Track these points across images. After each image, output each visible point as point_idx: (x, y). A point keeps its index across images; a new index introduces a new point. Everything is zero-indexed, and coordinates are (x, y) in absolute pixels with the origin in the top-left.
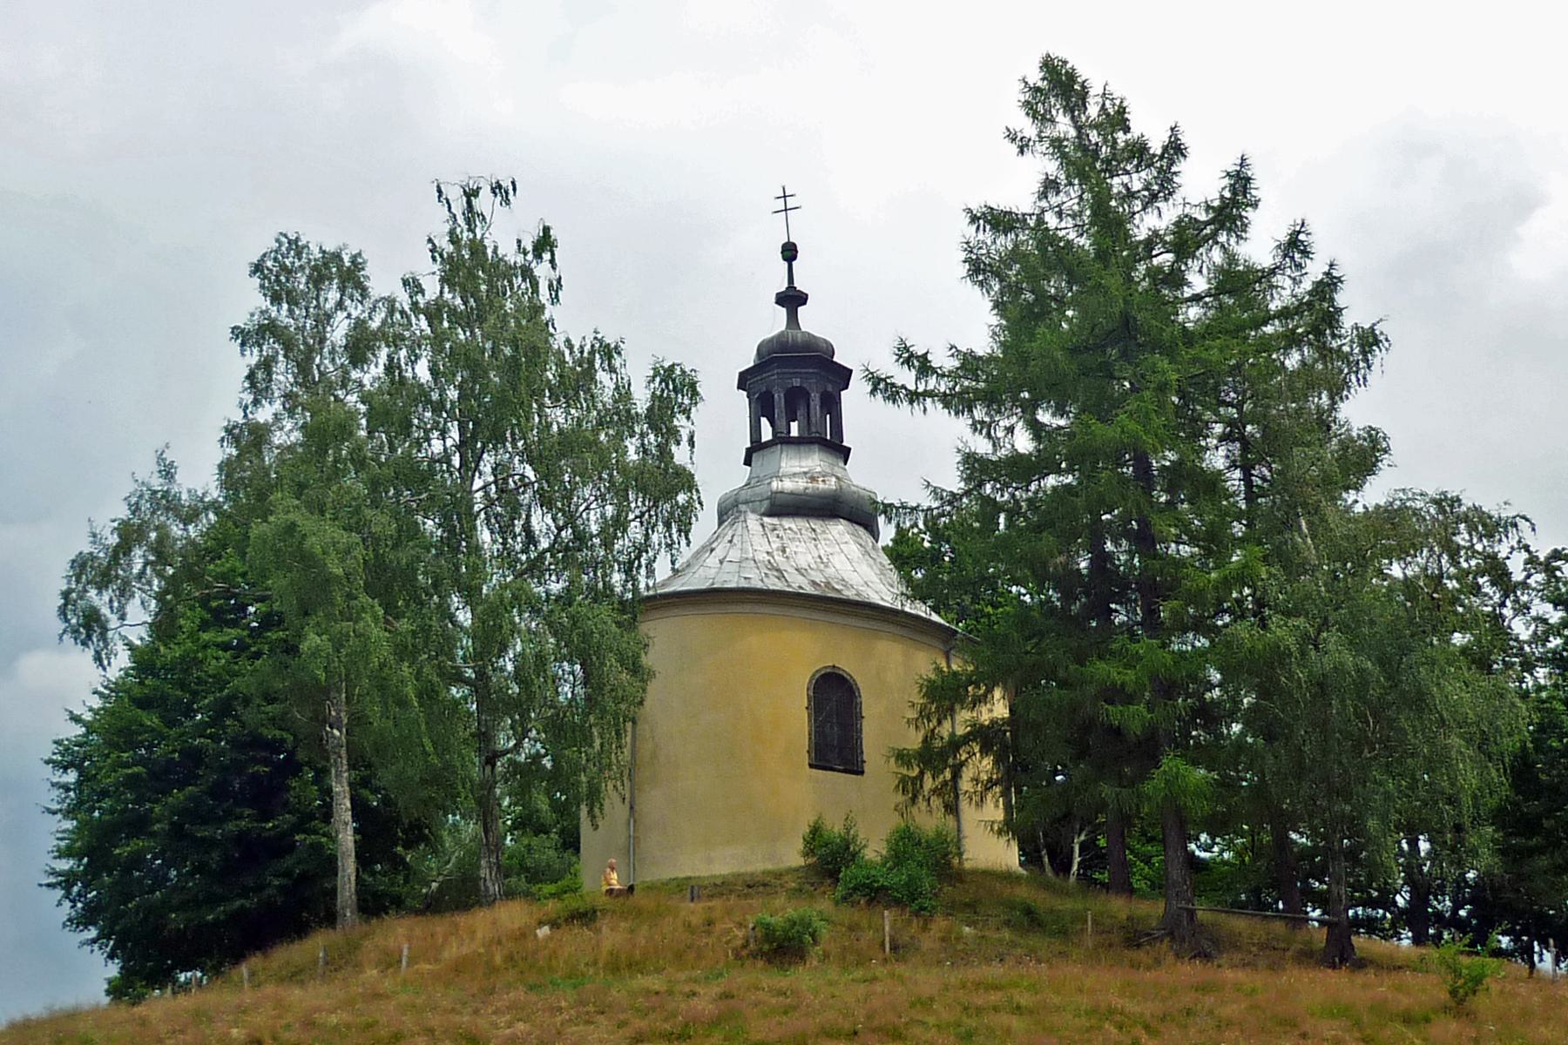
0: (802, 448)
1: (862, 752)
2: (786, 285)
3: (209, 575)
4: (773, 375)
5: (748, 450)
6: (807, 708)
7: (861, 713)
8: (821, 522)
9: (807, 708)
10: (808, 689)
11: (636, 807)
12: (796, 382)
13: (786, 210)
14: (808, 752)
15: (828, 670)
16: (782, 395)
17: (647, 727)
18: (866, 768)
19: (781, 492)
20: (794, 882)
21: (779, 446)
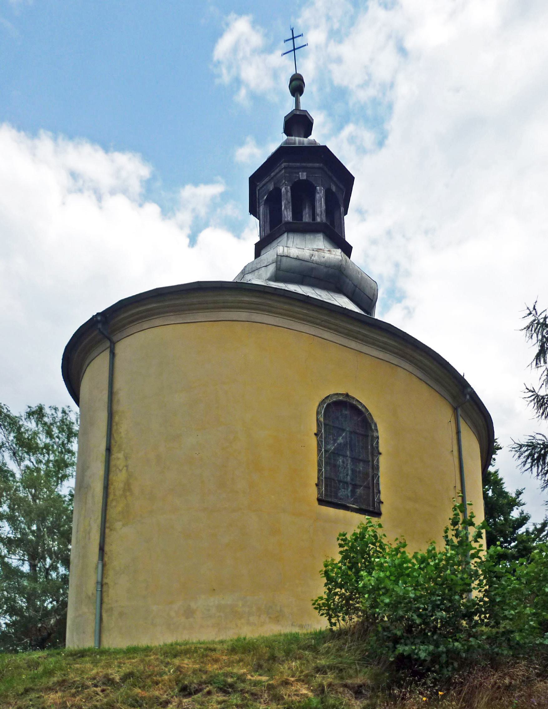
0: (308, 237)
1: (379, 492)
2: (294, 108)
3: (403, 625)
4: (280, 171)
5: (257, 245)
6: (316, 434)
7: (378, 447)
8: (328, 294)
9: (316, 434)
10: (318, 413)
11: (107, 549)
12: (303, 176)
13: (294, 49)
14: (317, 485)
15: (341, 398)
16: (289, 187)
17: (121, 455)
18: (384, 509)
19: (287, 256)
20: (306, 680)
21: (286, 235)
